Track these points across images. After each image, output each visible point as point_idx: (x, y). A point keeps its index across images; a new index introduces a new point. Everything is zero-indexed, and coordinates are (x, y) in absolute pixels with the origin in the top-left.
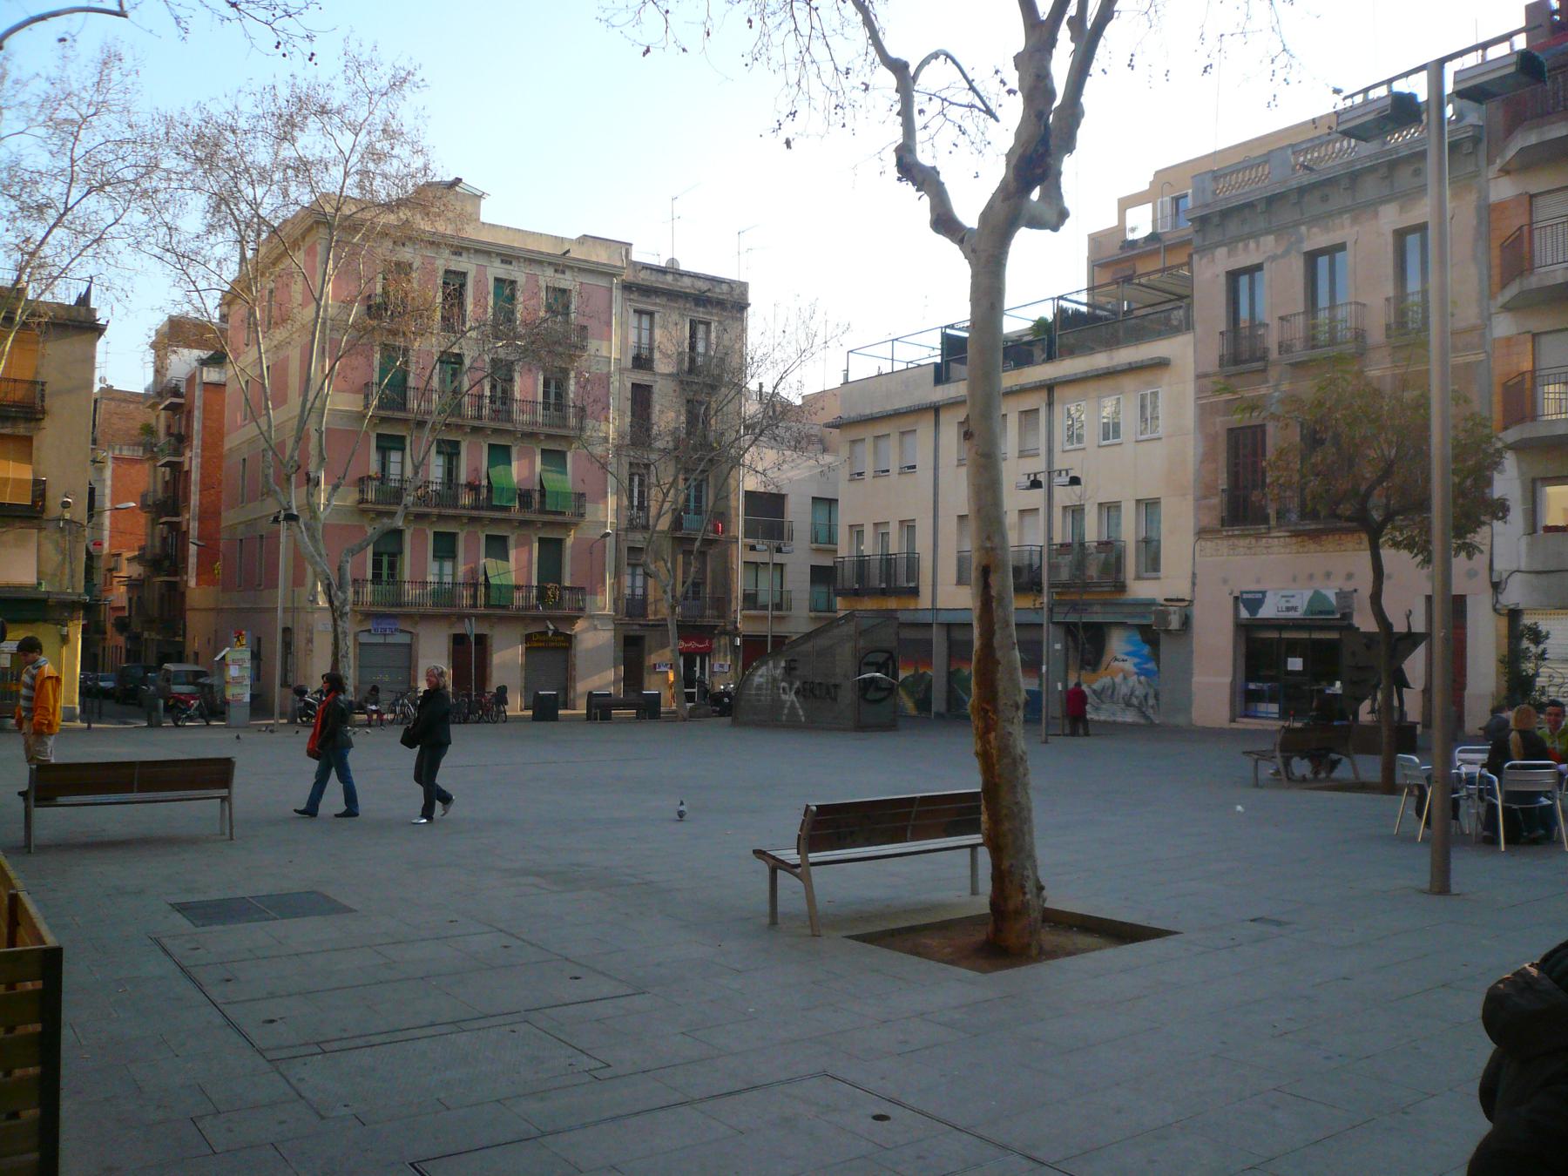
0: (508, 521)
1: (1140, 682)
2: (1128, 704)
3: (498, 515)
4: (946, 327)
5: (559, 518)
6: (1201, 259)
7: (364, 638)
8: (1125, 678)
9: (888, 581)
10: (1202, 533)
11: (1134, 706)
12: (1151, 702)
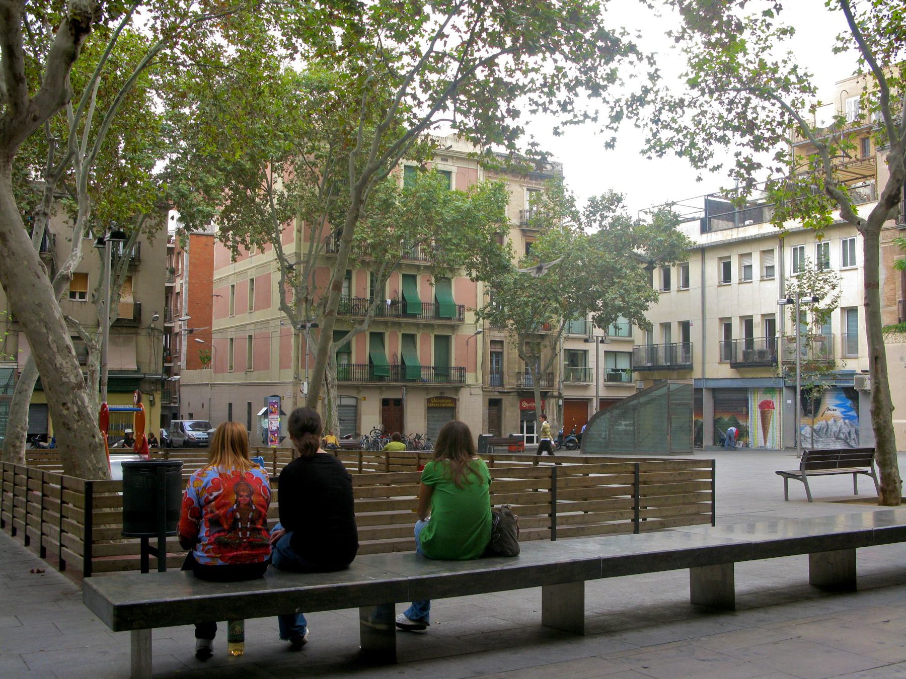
0: (417, 325)
1: (845, 423)
2: (838, 438)
3: (410, 320)
4: (708, 196)
5: (448, 322)
6: (882, 155)
8: (835, 421)
9: (671, 361)
11: (841, 439)
12: (853, 436)
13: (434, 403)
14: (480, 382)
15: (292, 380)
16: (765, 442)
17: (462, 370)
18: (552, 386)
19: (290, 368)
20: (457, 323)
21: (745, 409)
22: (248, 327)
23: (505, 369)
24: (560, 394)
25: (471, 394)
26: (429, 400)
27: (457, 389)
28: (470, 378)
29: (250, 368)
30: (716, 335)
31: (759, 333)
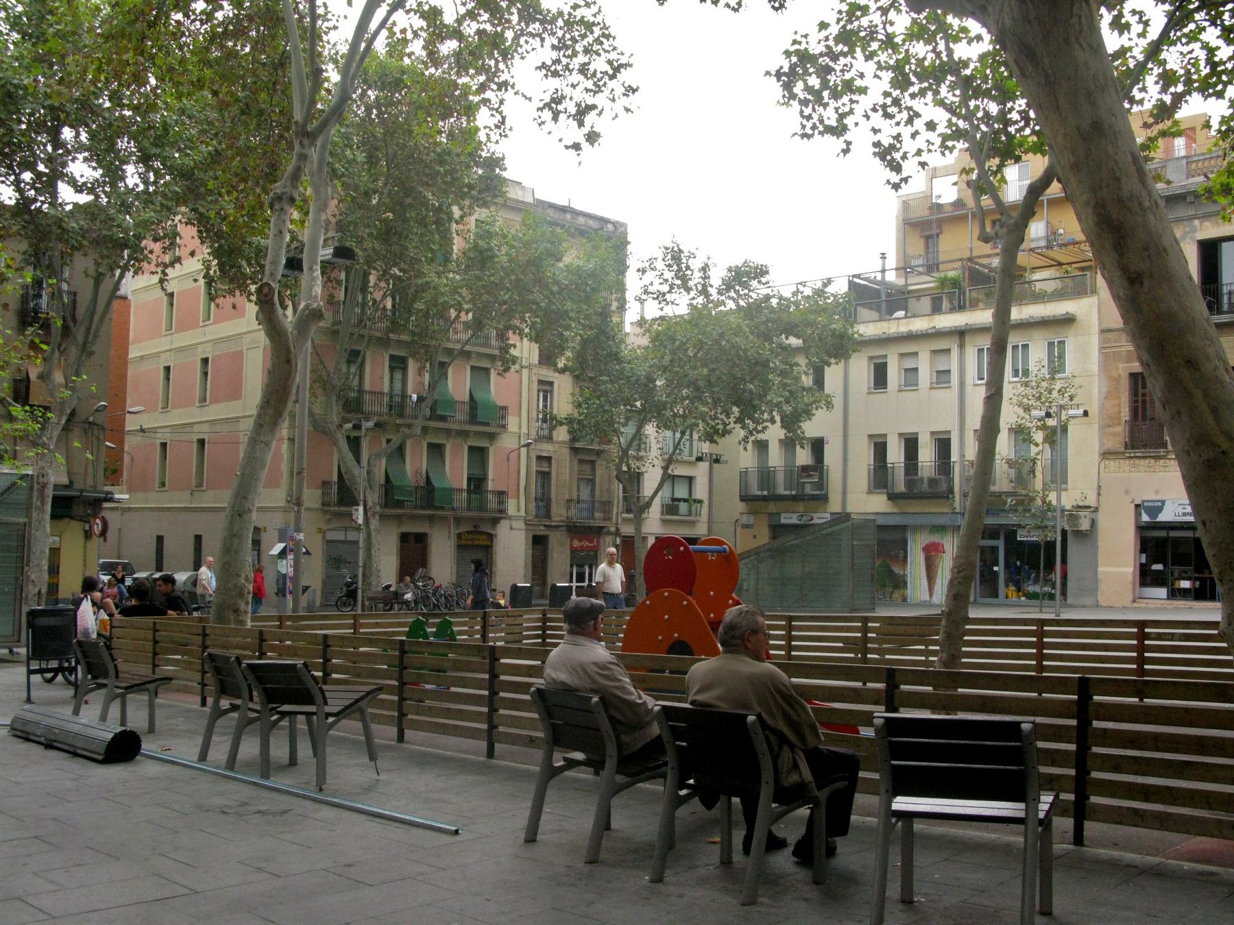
0: (448, 432)
4: (854, 276)
7: (331, 536)
10: (1106, 455)
13: (466, 540)
14: (522, 513)
15: (282, 504)
16: (931, 595)
17: (501, 494)
18: (609, 519)
19: (278, 486)
20: (498, 430)
21: (902, 553)
22: (196, 428)
23: (553, 496)
24: (618, 529)
25: (511, 528)
26: (459, 536)
27: (495, 521)
28: (511, 507)
29: (200, 484)
30: (863, 458)
31: (927, 455)
